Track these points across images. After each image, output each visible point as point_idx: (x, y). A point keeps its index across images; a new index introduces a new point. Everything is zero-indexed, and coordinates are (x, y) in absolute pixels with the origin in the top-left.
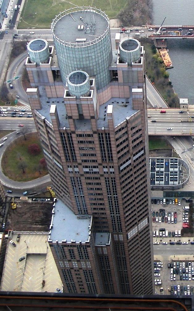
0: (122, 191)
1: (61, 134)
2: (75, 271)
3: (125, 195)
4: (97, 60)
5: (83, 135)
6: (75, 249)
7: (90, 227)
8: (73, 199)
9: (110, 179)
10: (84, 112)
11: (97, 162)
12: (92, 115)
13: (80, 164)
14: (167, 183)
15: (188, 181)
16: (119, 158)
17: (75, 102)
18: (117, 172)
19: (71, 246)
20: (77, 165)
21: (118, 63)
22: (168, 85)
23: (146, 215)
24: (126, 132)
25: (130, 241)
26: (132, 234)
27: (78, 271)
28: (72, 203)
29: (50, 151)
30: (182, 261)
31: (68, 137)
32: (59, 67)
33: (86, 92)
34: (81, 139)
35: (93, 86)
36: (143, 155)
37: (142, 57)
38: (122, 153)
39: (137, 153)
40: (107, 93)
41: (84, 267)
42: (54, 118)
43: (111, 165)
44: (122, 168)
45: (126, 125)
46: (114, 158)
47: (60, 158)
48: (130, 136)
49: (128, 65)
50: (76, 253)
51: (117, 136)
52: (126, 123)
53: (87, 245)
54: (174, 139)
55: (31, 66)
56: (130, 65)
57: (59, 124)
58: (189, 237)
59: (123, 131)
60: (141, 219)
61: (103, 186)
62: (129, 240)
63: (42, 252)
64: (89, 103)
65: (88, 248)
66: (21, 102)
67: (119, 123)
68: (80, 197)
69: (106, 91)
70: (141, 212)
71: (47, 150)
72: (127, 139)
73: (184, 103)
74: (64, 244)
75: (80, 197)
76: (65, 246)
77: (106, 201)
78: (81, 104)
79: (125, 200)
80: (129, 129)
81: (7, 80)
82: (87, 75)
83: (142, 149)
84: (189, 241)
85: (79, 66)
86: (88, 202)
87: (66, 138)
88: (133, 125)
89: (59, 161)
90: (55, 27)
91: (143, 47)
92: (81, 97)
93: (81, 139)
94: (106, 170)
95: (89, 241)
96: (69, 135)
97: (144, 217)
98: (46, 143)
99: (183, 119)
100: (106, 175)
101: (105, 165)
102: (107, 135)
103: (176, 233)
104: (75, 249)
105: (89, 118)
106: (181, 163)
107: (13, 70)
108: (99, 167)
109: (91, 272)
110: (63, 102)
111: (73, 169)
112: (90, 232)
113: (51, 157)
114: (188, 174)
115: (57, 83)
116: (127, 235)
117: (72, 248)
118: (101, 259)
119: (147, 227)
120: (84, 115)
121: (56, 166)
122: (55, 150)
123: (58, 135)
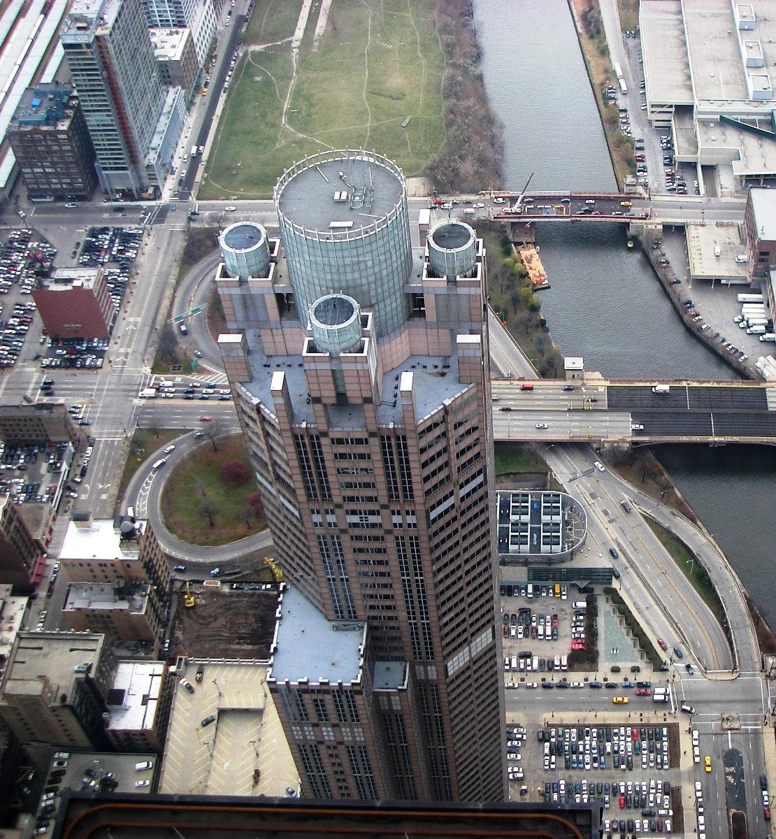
0: (435, 568)
1: (296, 437)
2: (329, 747)
3: (441, 576)
4: (377, 269)
5: (347, 440)
6: (328, 698)
7: (362, 648)
8: (324, 584)
10: (348, 387)
11: (376, 501)
12: (366, 394)
13: (339, 506)
14: (535, 548)
15: (584, 543)
16: (428, 493)
17: (327, 366)
18: (423, 525)
19: (319, 691)
21: (424, 278)
22: (537, 326)
23: (489, 621)
24: (444, 434)
25: (452, 681)
26: (456, 663)
27: (335, 747)
29: (271, 477)
31: (313, 445)
32: (292, 286)
33: (352, 342)
34: (341, 449)
35: (368, 328)
36: (481, 485)
37: (479, 264)
38: (435, 480)
39: (467, 482)
40: (400, 345)
41: (347, 738)
42: (281, 401)
43: (409, 508)
44: (433, 515)
46: (416, 493)
47: (293, 491)
48: (452, 442)
50: (330, 707)
51: (423, 443)
52: (442, 413)
53: (355, 690)
54: (552, 450)
55: (228, 285)
56: (452, 282)
57: (291, 416)
58: (585, 670)
59: (437, 432)
60: (478, 630)
61: (392, 556)
62: (450, 679)
63: (253, 706)
64: (360, 367)
65: (357, 697)
66: (205, 366)
67: (427, 412)
68: (338, 580)
69: (398, 340)
70: (477, 616)
71: (265, 474)
73: (574, 367)
75: (338, 580)
76: (306, 691)
77: (398, 590)
78: (342, 371)
79: (442, 587)
80: (451, 426)
81: (175, 315)
82: (356, 305)
83: (479, 472)
85: (336, 285)
86: (356, 591)
87: (308, 448)
88: (460, 417)
90: (282, 195)
91: (481, 240)
92: (342, 355)
94: (397, 519)
95: (358, 681)
97: (483, 626)
98: (261, 459)
99: (571, 405)
100: (398, 532)
101: (396, 508)
102: (401, 439)
103: (557, 663)
104: (328, 698)
105: (359, 401)
106: (569, 504)
108: (383, 512)
109: (364, 750)
110: (301, 365)
111: (404, 519)
112: (362, 660)
114: (584, 528)
115: (286, 323)
116: (446, 668)
117: (320, 697)
118: (387, 720)
119: (491, 649)
120: (349, 394)
121: (285, 511)
122: (282, 475)
123: (290, 441)
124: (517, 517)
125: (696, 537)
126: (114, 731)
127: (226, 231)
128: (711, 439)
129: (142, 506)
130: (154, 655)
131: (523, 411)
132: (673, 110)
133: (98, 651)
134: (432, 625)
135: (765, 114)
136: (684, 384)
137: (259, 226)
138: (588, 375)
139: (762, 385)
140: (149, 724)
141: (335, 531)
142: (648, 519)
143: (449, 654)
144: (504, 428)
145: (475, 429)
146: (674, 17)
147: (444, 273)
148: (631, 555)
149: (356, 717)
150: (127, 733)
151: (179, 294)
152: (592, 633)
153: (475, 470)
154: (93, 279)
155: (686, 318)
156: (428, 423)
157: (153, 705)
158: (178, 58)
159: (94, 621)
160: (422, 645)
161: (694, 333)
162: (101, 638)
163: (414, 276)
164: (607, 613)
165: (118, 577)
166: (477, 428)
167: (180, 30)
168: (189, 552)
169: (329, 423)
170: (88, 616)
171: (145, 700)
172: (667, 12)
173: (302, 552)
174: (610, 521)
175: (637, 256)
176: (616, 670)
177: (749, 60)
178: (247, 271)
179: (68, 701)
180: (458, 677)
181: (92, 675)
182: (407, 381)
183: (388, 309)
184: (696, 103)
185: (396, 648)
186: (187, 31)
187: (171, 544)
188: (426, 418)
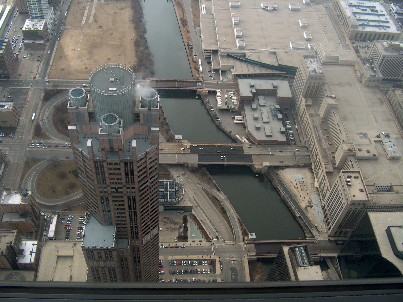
0: (140, 207)
1: (95, 162)
3: (142, 209)
4: (124, 105)
7: (114, 235)
8: (102, 213)
9: (131, 198)
10: (114, 145)
12: (120, 148)
13: (109, 186)
15: (183, 198)
16: (139, 181)
17: (107, 138)
18: (137, 192)
19: (99, 250)
20: (106, 186)
22: (166, 124)
23: (157, 225)
24: (146, 162)
25: (144, 246)
26: (146, 239)
27: (104, 268)
28: (100, 216)
29: (85, 176)
30: (195, 260)
31: (101, 165)
32: (94, 110)
33: (116, 130)
35: (121, 125)
37: (159, 104)
38: (142, 177)
39: (152, 178)
40: (131, 131)
42: (90, 149)
43: (133, 186)
44: (141, 189)
45: (146, 156)
46: (135, 181)
47: (93, 181)
48: (148, 164)
49: (148, 110)
51: (139, 165)
52: (145, 154)
53: (112, 249)
54: (171, 166)
56: (149, 109)
57: (94, 155)
58: (183, 241)
59: (143, 161)
60: (153, 228)
61: (126, 203)
62: (144, 245)
63: (69, 255)
64: (118, 138)
65: (113, 251)
66: (52, 137)
67: (140, 155)
68: (107, 211)
69: (130, 129)
71: (82, 175)
72: (146, 167)
73: (178, 138)
74: (94, 248)
75: (107, 211)
77: (127, 214)
78: (112, 139)
79: (142, 213)
80: (148, 159)
81: (40, 119)
82: (117, 117)
84: (169, 245)
85: (110, 110)
86: (113, 215)
87: (99, 165)
88: (151, 156)
89: (92, 184)
90: (92, 78)
91: (159, 96)
92: (112, 134)
93: (111, 166)
95: (113, 246)
96: (101, 163)
97: (155, 227)
98: (81, 169)
99: (178, 151)
100: (128, 195)
101: (128, 186)
102: (132, 164)
104: (102, 252)
105: (118, 150)
106: (177, 185)
107: (44, 111)
108: (124, 188)
109: (114, 269)
110: (96, 138)
112: (114, 239)
113: (85, 181)
114: (183, 193)
116: (142, 241)
117: (100, 251)
118: (122, 260)
119: (157, 235)
121: (89, 187)
122: (89, 175)
123: (93, 163)
124: (171, 189)
125: (221, 196)
126: (20, 264)
127: (71, 91)
128: (225, 163)
129: (29, 186)
130: (33, 237)
131: (168, 153)
132: (211, 52)
133: (14, 236)
134: (138, 226)
135: (242, 54)
136: (216, 144)
137: (83, 89)
138: (183, 141)
139: (242, 145)
140: (33, 261)
141: (106, 194)
142: (204, 189)
143: (143, 237)
144: (163, 159)
145: (155, 160)
146: (212, 20)
147: (147, 106)
148: (198, 202)
149: (112, 258)
150: (25, 264)
151: (42, 111)
152: (186, 228)
153: (155, 174)
154: (12, 106)
155: (216, 122)
156: (141, 158)
157: (34, 255)
158: (41, 29)
159: (13, 226)
160: (135, 234)
161: (219, 128)
162: (15, 232)
163: (137, 106)
164: (191, 222)
165: (21, 210)
166: (156, 159)
167: (42, 20)
168: (45, 201)
169: (107, 158)
170: (10, 224)
171: (31, 253)
172: (208, 18)
173: (94, 201)
174: (191, 192)
175: (200, 101)
176: (194, 241)
177: (237, 35)
178: (78, 105)
179: (4, 254)
180: (146, 245)
181: (12, 245)
182: (134, 144)
183: (128, 118)
184: (219, 49)
185: (125, 235)
186: (44, 21)
187: (39, 199)
188: (140, 156)
